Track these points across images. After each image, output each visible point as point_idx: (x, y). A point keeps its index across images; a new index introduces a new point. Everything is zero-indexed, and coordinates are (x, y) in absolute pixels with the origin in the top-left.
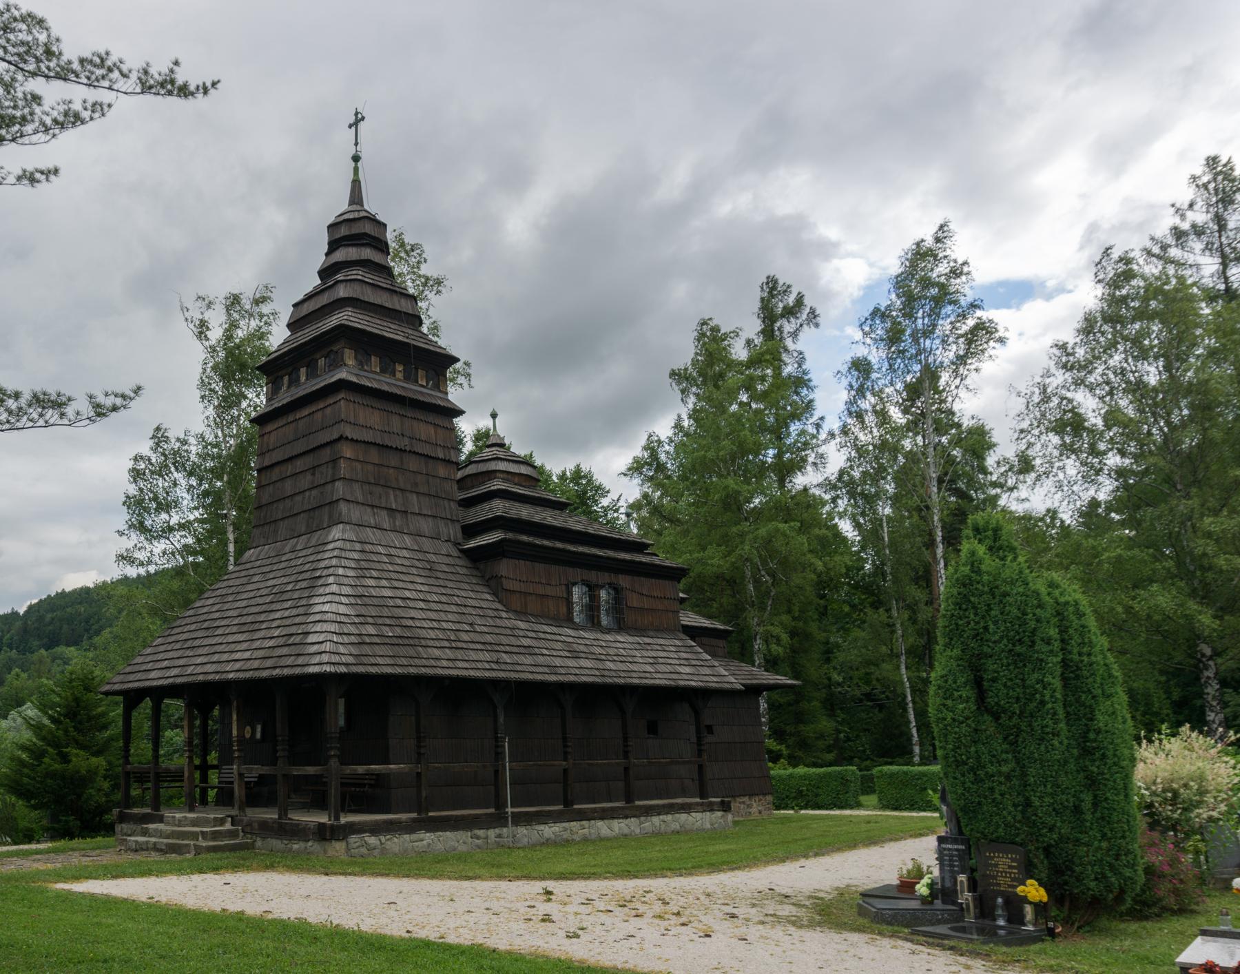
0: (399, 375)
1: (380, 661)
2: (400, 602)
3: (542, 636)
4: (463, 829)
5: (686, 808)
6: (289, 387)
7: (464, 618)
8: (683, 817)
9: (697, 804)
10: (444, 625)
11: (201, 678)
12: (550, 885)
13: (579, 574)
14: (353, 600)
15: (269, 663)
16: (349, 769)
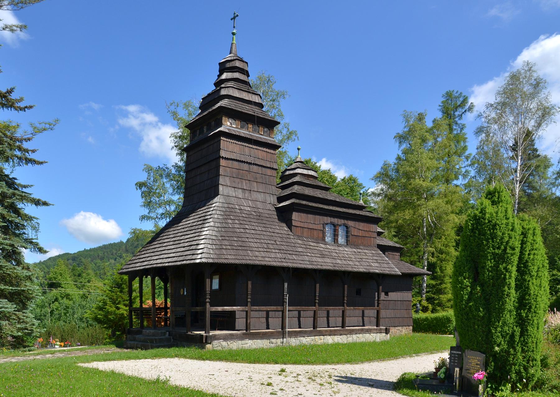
0: (251, 130)
1: (229, 257)
2: (242, 230)
3: (308, 247)
4: (266, 339)
5: (369, 331)
6: (199, 135)
7: (272, 238)
8: (367, 335)
9: (374, 329)
10: (262, 241)
11: (155, 266)
12: (284, 366)
13: (328, 219)
14: (220, 229)
15: (181, 258)
16: (214, 309)
